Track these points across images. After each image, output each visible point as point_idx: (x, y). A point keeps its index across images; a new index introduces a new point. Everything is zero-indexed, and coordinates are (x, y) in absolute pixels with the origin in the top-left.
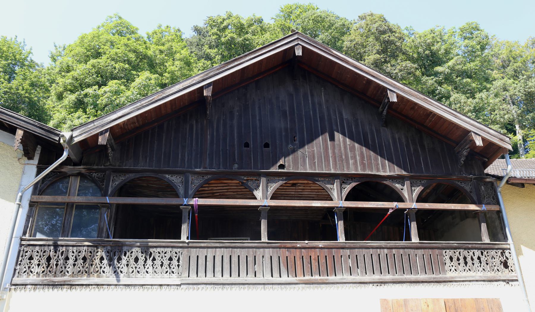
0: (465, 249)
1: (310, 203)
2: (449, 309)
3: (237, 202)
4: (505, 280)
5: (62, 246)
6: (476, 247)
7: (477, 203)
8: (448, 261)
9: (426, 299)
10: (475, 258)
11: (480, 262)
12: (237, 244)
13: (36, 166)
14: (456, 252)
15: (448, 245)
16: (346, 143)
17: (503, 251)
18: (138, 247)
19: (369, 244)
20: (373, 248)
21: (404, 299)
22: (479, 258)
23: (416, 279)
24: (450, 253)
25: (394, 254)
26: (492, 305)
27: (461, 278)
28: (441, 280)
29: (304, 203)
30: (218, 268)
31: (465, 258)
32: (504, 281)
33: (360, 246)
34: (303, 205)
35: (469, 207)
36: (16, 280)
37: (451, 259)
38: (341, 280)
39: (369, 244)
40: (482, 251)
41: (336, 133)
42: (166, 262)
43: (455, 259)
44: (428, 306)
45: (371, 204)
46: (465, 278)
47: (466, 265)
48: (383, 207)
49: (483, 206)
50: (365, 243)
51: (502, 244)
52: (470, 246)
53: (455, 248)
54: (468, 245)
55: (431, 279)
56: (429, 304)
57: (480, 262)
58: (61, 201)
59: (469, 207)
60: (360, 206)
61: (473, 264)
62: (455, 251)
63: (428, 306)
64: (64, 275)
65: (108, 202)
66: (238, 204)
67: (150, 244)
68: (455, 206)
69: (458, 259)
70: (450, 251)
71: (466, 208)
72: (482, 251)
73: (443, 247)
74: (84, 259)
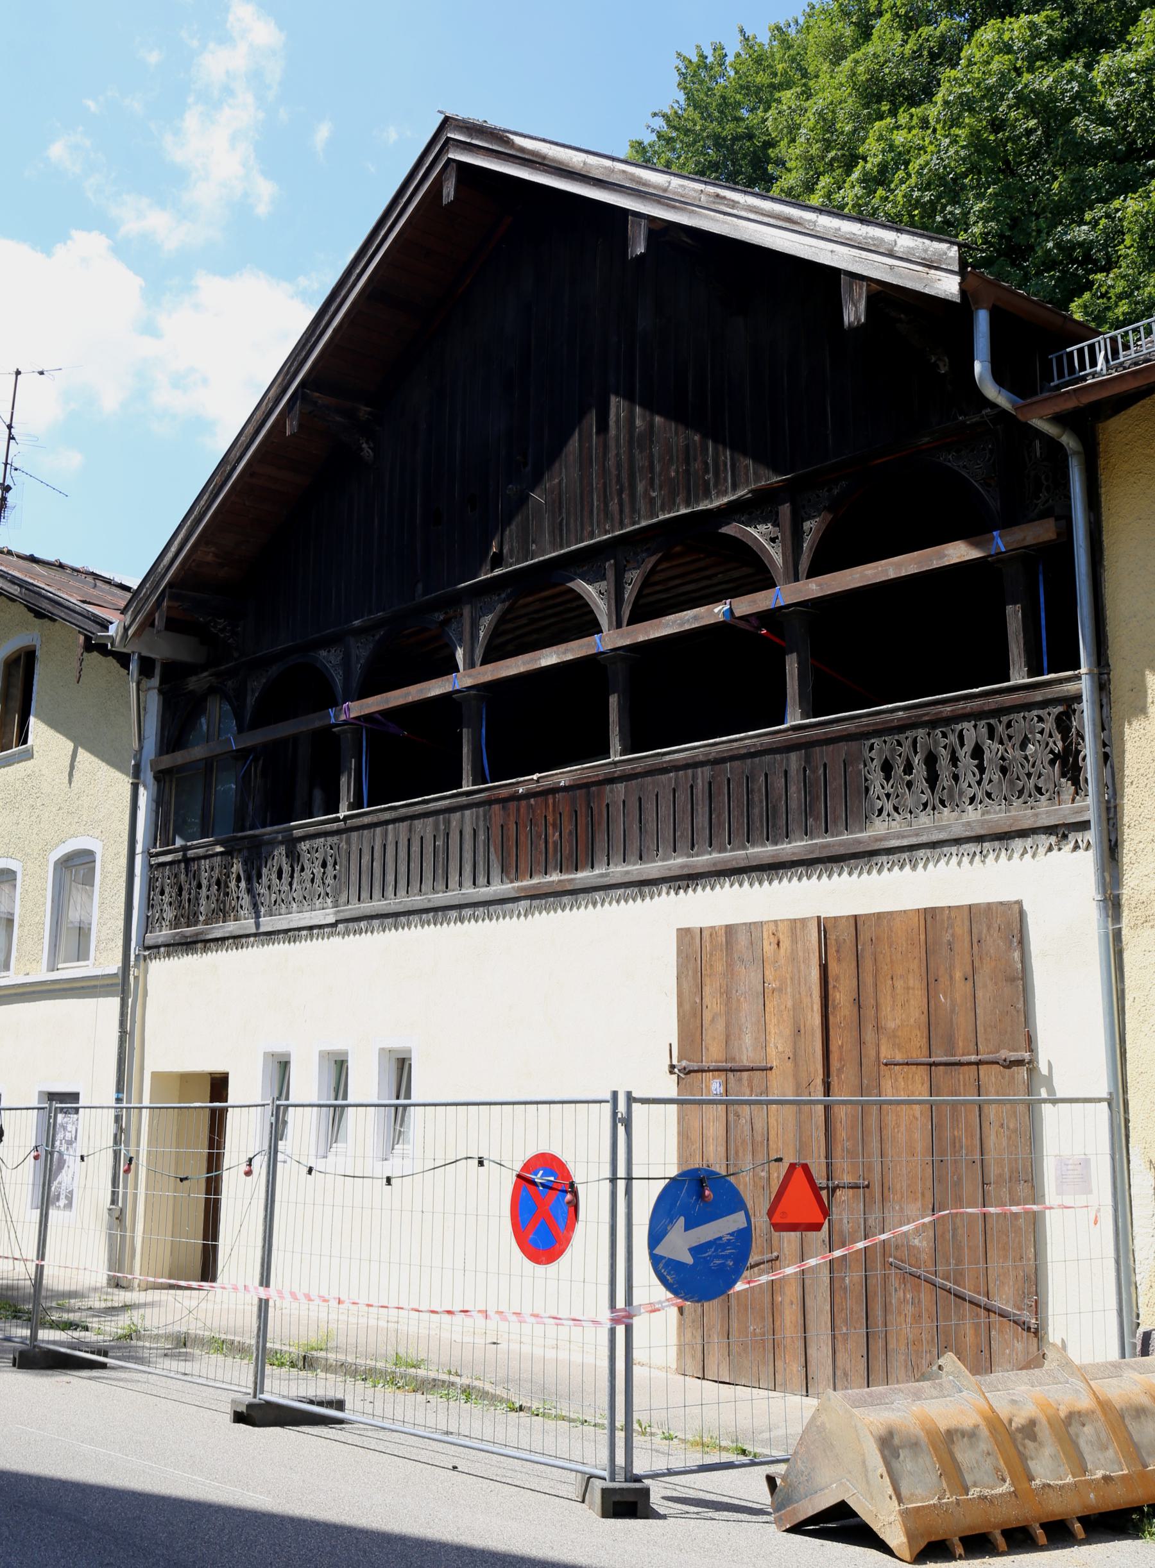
0: (933, 724)
1: (536, 660)
2: (837, 951)
3: (408, 694)
4: (1056, 826)
5: (199, 858)
6: (968, 710)
7: (179, 758)
8: (877, 777)
9: (776, 922)
10: (964, 753)
11: (982, 769)
12: (417, 808)
13: (156, 691)
14: (903, 740)
15: (878, 719)
16: (634, 422)
17: (1069, 706)
18: (282, 843)
19: (668, 758)
20: (676, 767)
21: (727, 926)
22: (977, 753)
23: (773, 856)
24: (880, 748)
25: (729, 780)
26: (985, 931)
27: (903, 837)
28: (842, 851)
29: (524, 663)
30: (403, 882)
31: (931, 760)
32: (1049, 830)
33: (648, 768)
34: (522, 669)
35: (945, 556)
36: (151, 939)
37: (887, 768)
38: (599, 879)
39: (668, 758)
40: (992, 721)
41: (614, 400)
42: (319, 871)
43: (898, 770)
44: (778, 944)
45: (667, 625)
46: (917, 835)
47: (932, 788)
48: (696, 625)
49: (993, 538)
50: (658, 754)
51: (1060, 681)
52: (947, 709)
53: (902, 728)
54: (940, 708)
55: (812, 852)
56: (781, 937)
57: (982, 769)
58: (895, 576)
59: (945, 556)
60: (641, 638)
61: (956, 778)
62: (901, 737)
63: (778, 944)
64: (196, 923)
65: (1003, 550)
66: (410, 699)
67: (297, 833)
68: (898, 566)
69: (908, 769)
70: (885, 742)
71: (936, 564)
72: (992, 721)
73: (862, 729)
74: (218, 883)
